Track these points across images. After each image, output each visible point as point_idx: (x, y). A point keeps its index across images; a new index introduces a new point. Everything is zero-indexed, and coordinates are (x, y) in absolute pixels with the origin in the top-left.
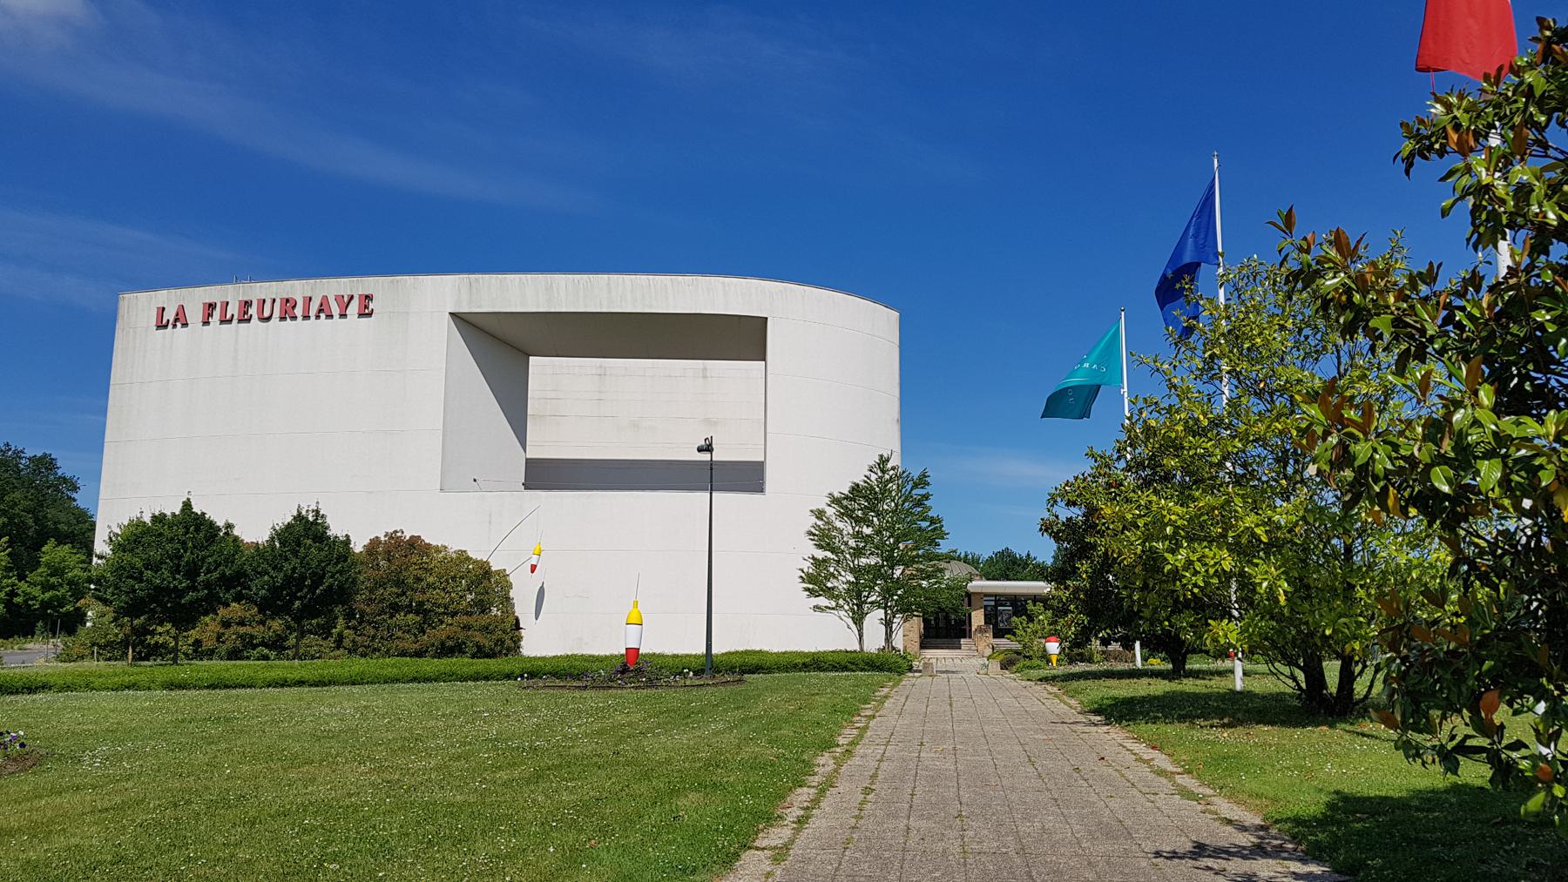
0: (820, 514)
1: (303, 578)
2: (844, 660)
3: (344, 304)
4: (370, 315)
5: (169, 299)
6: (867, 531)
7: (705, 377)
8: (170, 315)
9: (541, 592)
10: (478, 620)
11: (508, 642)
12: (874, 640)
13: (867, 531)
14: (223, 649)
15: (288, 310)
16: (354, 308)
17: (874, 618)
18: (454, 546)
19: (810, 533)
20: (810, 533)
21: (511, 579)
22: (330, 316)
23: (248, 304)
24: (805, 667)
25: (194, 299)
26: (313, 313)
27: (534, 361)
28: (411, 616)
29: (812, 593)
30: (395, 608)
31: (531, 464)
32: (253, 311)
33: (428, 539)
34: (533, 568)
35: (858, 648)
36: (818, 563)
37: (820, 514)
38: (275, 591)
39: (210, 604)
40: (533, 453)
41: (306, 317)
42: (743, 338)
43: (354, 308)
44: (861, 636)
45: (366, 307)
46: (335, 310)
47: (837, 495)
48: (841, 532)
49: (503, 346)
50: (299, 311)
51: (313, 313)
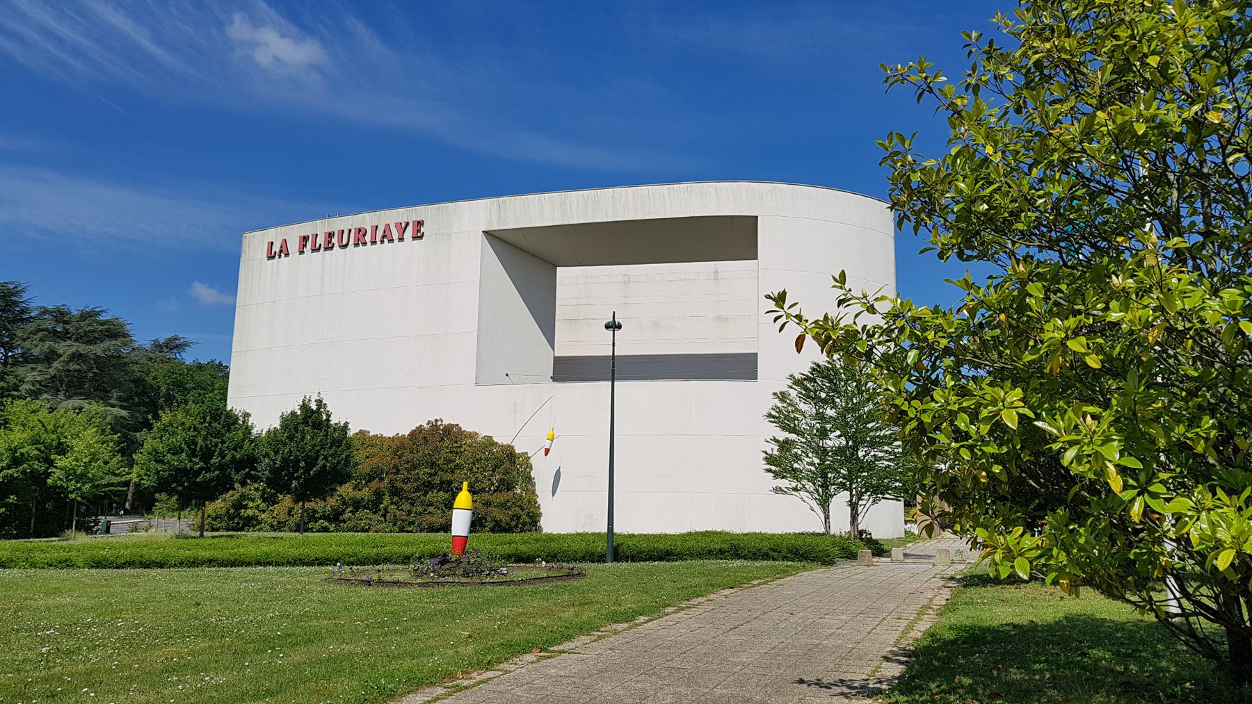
0: (783, 397)
1: (297, 461)
2: (765, 546)
3: (402, 229)
4: (421, 237)
5: (275, 235)
6: (830, 412)
7: (717, 279)
8: (276, 248)
9: (558, 474)
10: (501, 497)
11: (525, 518)
12: (840, 523)
13: (830, 412)
14: (292, 521)
15: (360, 237)
16: (409, 232)
17: (840, 501)
18: (483, 432)
19: (770, 416)
20: (770, 416)
21: (532, 461)
22: (391, 241)
23: (331, 235)
24: (721, 554)
25: (293, 233)
26: (378, 239)
27: (566, 276)
28: (441, 493)
29: (777, 475)
30: (429, 486)
31: (558, 361)
32: (335, 240)
33: (465, 427)
34: (547, 452)
35: (822, 530)
36: (785, 445)
37: (783, 397)
38: (275, 472)
39: (224, 485)
40: (561, 352)
41: (374, 243)
42: (734, 238)
43: (409, 232)
44: (827, 518)
45: (418, 231)
46: (395, 235)
47: (798, 376)
48: (803, 414)
49: (532, 260)
50: (368, 238)
51: (378, 239)
